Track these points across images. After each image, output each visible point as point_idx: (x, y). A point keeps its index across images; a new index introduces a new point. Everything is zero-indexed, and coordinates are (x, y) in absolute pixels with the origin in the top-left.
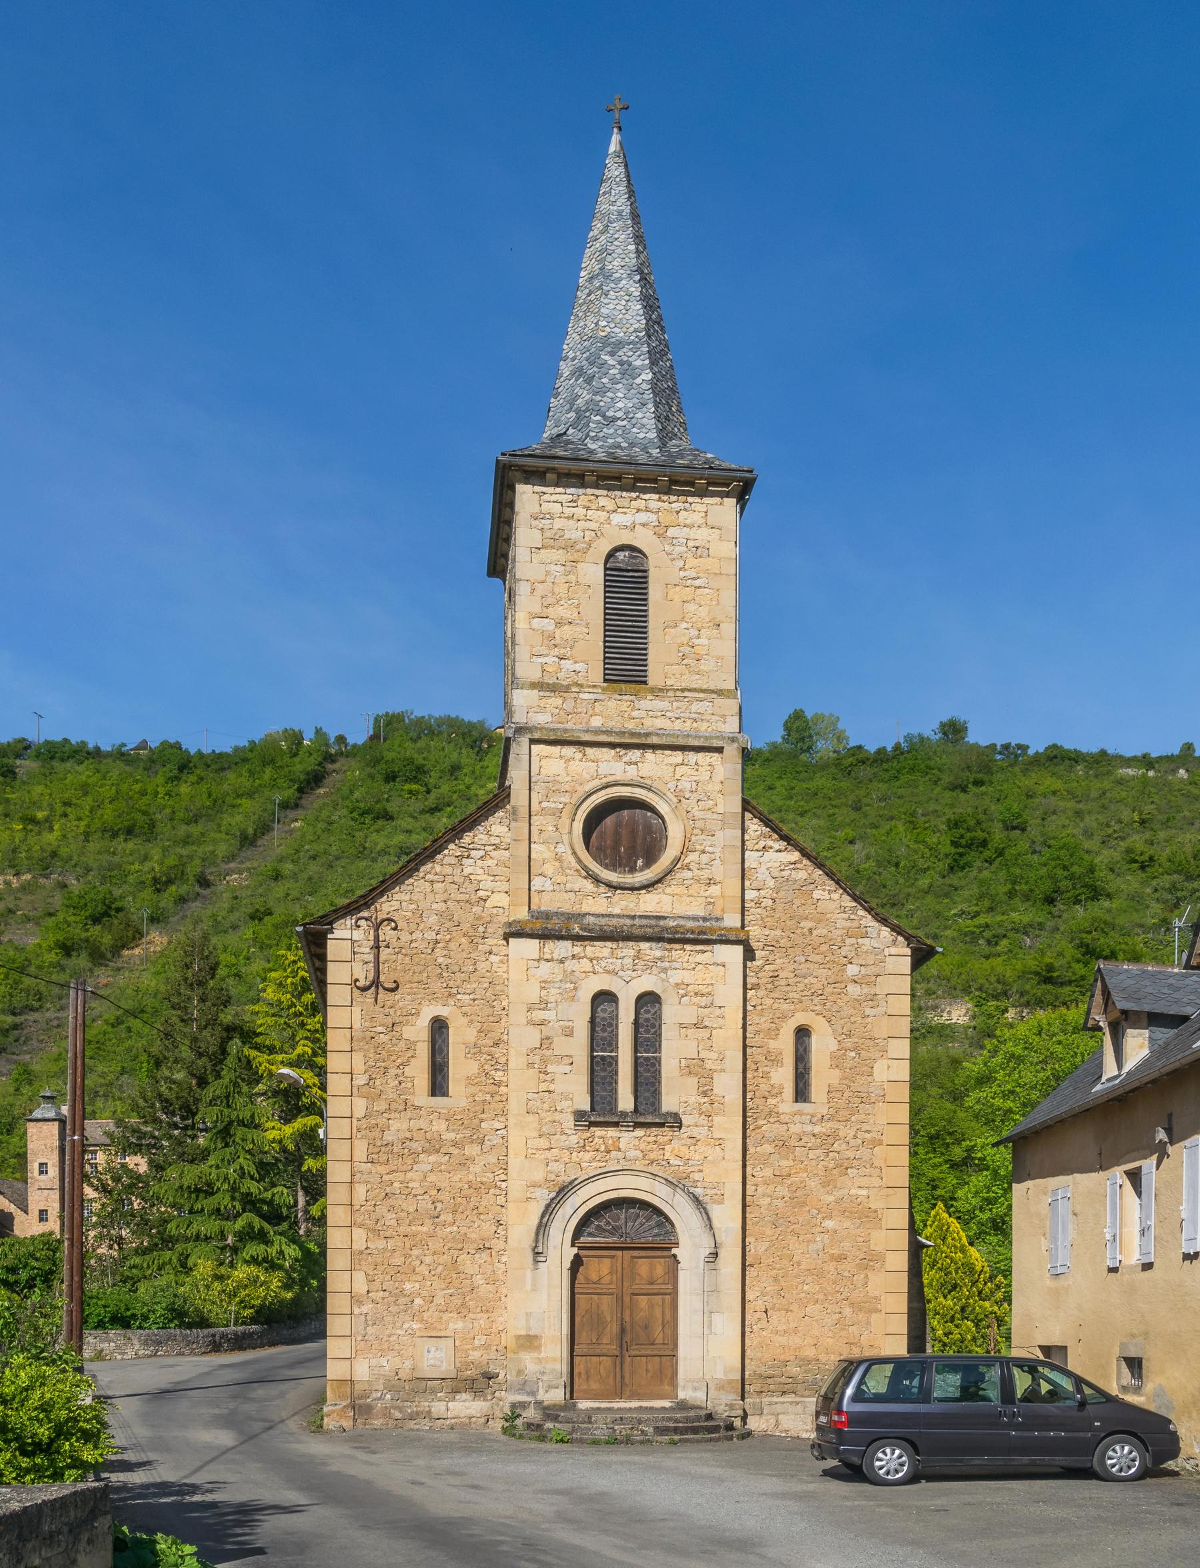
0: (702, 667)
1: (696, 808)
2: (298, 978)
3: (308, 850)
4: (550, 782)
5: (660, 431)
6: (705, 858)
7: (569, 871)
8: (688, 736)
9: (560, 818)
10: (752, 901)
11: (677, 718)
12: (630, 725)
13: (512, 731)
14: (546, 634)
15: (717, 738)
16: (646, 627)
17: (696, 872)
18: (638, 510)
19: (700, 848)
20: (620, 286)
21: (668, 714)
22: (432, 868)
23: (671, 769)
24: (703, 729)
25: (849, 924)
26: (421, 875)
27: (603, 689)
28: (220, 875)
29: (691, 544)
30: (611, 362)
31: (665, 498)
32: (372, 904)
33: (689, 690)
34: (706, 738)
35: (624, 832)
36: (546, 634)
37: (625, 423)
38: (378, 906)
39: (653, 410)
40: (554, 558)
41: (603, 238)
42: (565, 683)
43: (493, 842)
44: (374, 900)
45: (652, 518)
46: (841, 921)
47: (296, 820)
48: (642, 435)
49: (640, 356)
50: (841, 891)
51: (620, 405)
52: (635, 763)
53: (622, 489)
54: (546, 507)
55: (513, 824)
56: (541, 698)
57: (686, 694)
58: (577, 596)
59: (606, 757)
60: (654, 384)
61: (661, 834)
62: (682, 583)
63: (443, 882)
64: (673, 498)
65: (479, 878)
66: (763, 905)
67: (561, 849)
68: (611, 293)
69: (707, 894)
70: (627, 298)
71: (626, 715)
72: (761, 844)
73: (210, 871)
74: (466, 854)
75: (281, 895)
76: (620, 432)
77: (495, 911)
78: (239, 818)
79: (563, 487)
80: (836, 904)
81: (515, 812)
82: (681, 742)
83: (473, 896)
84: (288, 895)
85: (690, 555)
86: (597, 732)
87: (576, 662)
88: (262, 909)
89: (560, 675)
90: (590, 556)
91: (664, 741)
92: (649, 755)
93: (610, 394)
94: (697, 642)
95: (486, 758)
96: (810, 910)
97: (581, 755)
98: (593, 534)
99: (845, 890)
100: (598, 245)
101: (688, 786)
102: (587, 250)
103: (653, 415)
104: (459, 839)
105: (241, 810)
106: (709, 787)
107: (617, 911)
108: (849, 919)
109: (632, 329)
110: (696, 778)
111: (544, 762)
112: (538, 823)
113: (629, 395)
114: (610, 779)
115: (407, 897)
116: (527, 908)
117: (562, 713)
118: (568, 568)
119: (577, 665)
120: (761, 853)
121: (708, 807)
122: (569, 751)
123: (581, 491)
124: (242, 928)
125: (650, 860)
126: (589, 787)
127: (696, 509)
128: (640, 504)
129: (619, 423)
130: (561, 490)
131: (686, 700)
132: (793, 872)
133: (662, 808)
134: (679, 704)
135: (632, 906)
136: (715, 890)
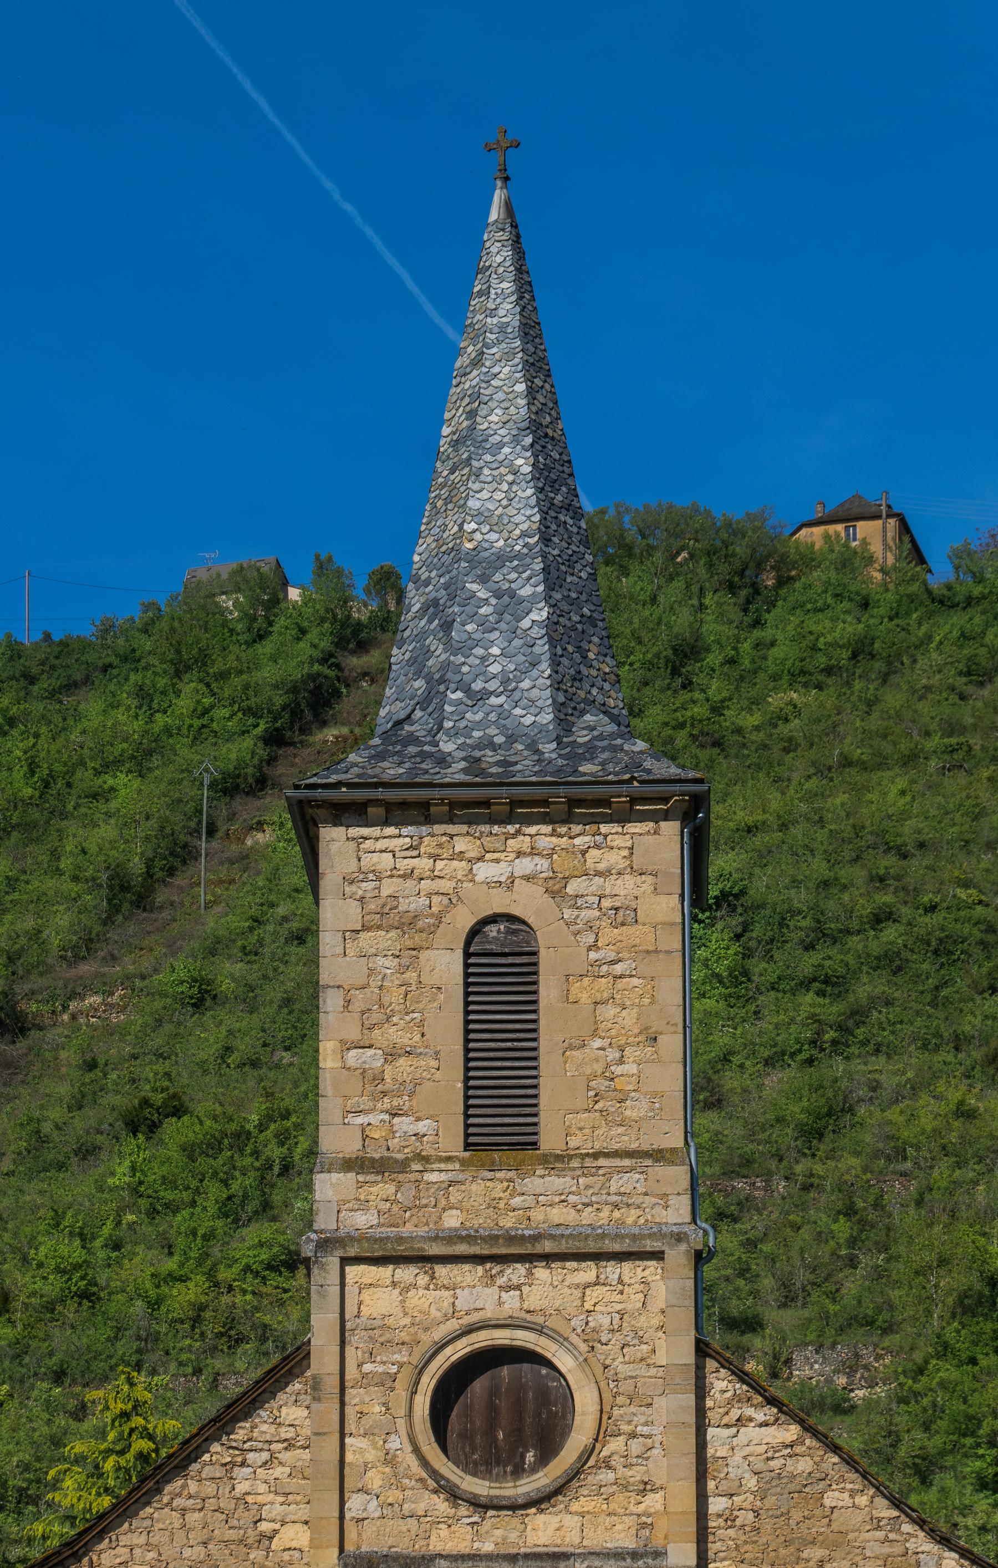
0: (628, 1113)
1: (621, 1359)
2: (130, 1456)
3: (285, 919)
4: (380, 1326)
5: (558, 707)
6: (636, 1446)
7: (407, 1481)
8: (603, 1236)
9: (393, 1389)
10: (719, 1516)
11: (586, 1205)
12: (508, 1222)
13: (312, 1246)
14: (369, 1074)
15: (652, 1236)
16: (535, 1049)
17: (621, 1471)
18: (519, 854)
19: (625, 1428)
20: (501, 457)
21: (572, 1198)
22: (184, 1486)
23: (577, 1293)
24: (630, 1221)
25: (886, 1549)
26: (165, 1500)
27: (463, 1162)
28: (53, 998)
29: (606, 903)
30: (482, 594)
31: (563, 829)
32: (85, 1554)
33: (607, 1155)
34: (634, 1237)
35: (503, 1404)
36: (369, 1074)
37: (502, 699)
38: (95, 1558)
39: (548, 672)
40: (381, 946)
41: (475, 373)
42: (400, 1156)
43: (283, 1436)
44: (87, 1549)
45: (543, 864)
46: (873, 1543)
47: (260, 826)
48: (529, 720)
49: (530, 578)
50: (872, 1491)
51: (495, 669)
52: (518, 1287)
53: (492, 820)
54: (368, 861)
55: (315, 1406)
56: (360, 1185)
57: (602, 1162)
58: (421, 1006)
59: (469, 1279)
60: (551, 625)
61: (564, 1407)
62: (593, 971)
63: (201, 1510)
64: (577, 829)
65: (260, 1499)
66: (738, 1522)
67: (394, 1443)
68: (486, 471)
69: (641, 1508)
70: (510, 478)
71: (502, 1205)
72: (735, 1414)
73: (27, 987)
74: (239, 1459)
75: (209, 1052)
76: (493, 717)
77: (286, 1557)
78: (107, 831)
79: (396, 825)
80: (860, 1516)
81: (316, 1385)
82: (592, 1247)
83: (250, 1532)
84: (228, 1049)
85: (605, 922)
86: (454, 1237)
87: (418, 1119)
88: (158, 1099)
89: (394, 1143)
90: (440, 938)
91: (563, 1247)
92: (542, 1273)
93: (479, 651)
94: (619, 1070)
95: (770, 617)
96: (819, 1527)
97: (427, 1278)
98: (445, 900)
99: (878, 1489)
100: (467, 386)
101: (606, 1321)
102: (453, 390)
103: (548, 682)
104: (228, 1434)
105: (113, 805)
106: (642, 1321)
107: (488, 1547)
108: (886, 1540)
109: (517, 532)
110: (619, 1307)
111: (365, 1295)
112: (357, 1400)
113: (511, 650)
114: (475, 1317)
115: (142, 1540)
116: (336, 1551)
117: (395, 1208)
118: (405, 961)
119: (421, 1124)
120: (734, 1430)
121: (639, 1356)
122: (406, 1273)
123: (424, 829)
124: (104, 1155)
125: (547, 1452)
126: (438, 1334)
127: (614, 844)
128: (523, 843)
129: (494, 700)
130: (391, 830)
131: (601, 1172)
132: (789, 1462)
133: (564, 1362)
134: (590, 1180)
135: (513, 1536)
136: (653, 1501)
